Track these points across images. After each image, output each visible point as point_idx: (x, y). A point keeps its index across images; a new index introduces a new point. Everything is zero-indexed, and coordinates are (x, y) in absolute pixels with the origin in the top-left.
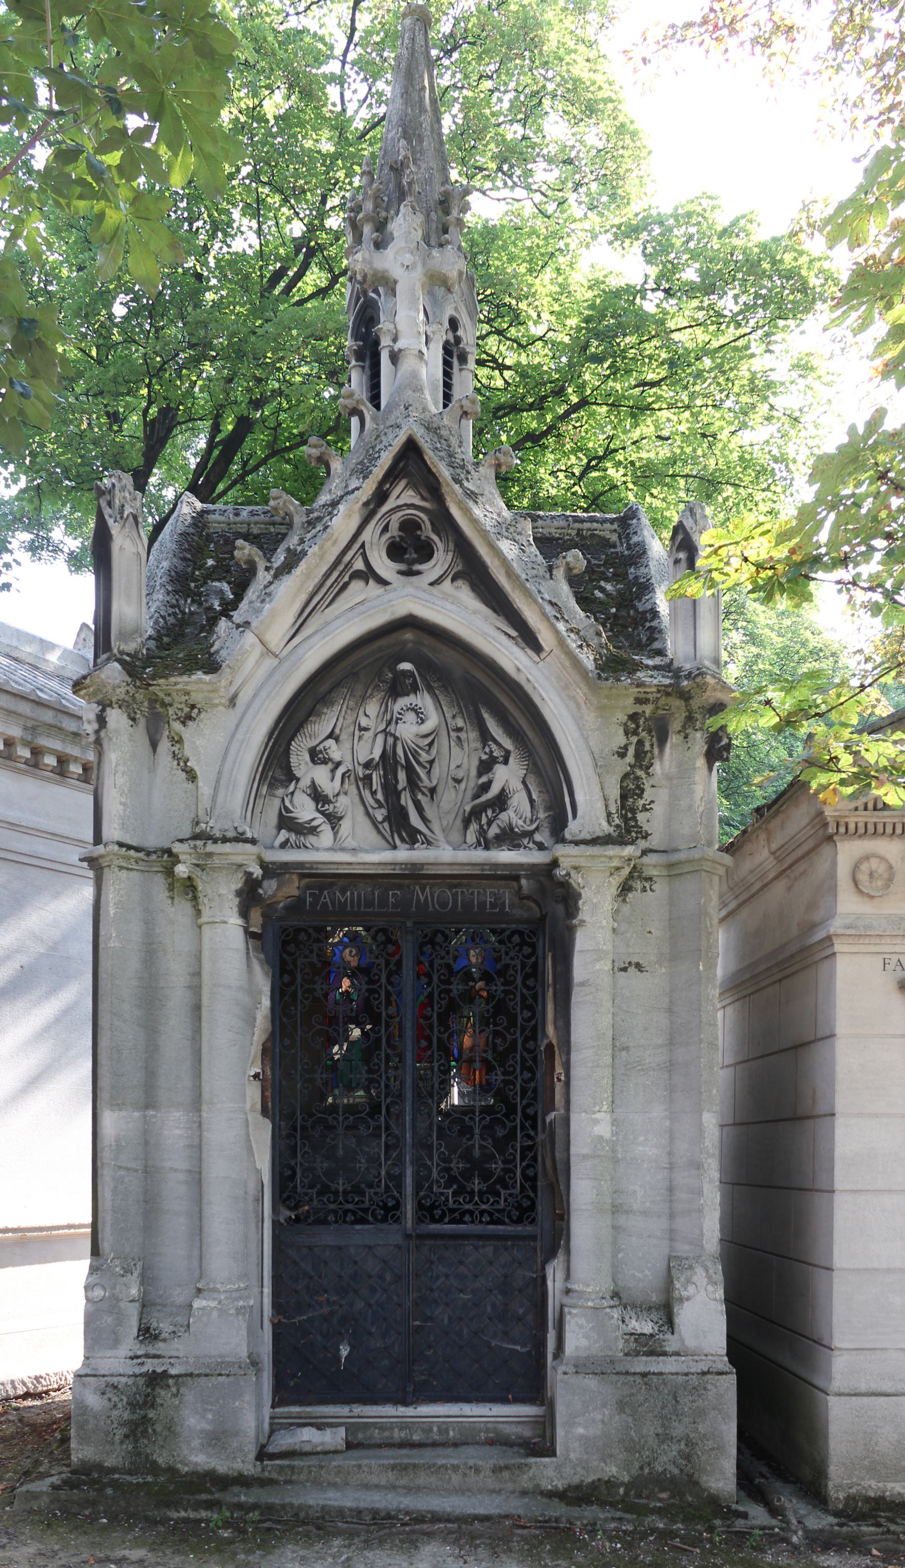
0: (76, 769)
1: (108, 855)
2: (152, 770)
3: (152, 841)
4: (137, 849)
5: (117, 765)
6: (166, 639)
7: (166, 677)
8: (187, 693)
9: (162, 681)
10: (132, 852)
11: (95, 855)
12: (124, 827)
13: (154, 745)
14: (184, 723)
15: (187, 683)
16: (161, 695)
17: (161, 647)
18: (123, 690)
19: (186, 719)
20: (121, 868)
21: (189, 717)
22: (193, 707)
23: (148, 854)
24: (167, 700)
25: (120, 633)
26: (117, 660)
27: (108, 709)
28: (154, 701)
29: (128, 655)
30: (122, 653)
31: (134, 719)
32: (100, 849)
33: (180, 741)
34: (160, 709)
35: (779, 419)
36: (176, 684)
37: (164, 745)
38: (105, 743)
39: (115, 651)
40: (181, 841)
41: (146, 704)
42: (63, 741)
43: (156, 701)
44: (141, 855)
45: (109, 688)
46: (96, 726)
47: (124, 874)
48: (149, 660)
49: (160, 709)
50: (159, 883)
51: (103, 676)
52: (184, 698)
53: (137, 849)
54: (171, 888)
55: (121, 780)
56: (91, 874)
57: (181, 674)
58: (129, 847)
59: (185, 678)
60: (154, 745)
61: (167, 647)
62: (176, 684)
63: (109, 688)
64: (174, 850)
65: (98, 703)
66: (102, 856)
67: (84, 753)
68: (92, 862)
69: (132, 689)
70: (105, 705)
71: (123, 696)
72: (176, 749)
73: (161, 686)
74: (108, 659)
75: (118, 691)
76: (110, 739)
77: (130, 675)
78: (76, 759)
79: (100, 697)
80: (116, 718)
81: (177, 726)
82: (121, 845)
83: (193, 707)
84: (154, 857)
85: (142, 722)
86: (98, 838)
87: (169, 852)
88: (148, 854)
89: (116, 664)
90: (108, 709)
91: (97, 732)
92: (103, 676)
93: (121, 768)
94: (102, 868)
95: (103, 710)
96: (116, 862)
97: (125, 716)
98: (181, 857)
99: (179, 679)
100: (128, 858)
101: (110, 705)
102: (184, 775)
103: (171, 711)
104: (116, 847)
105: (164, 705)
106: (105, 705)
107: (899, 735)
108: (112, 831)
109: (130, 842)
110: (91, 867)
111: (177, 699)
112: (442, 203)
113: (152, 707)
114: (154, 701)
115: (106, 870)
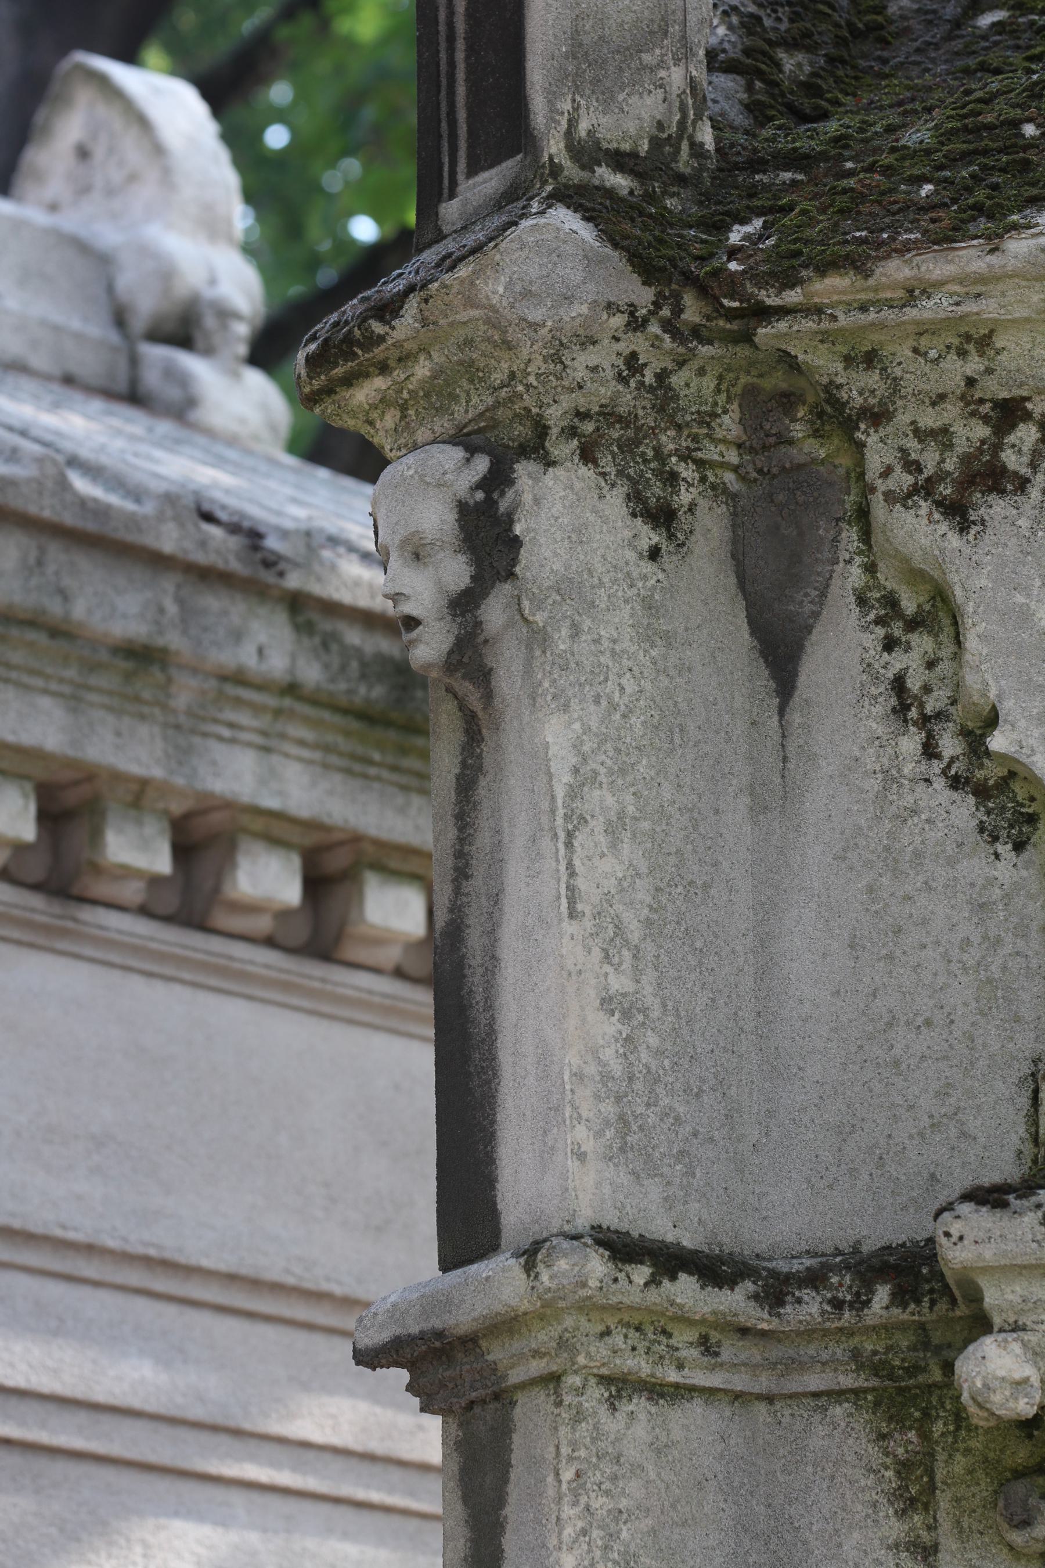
0: (137, 849)
1: (548, 1310)
2: (775, 795)
3: (791, 1216)
4: (714, 1269)
5: (582, 781)
6: (793, 64)
7: (857, 263)
8: (980, 341)
9: (832, 287)
10: (684, 1290)
11: (462, 1319)
12: (625, 1138)
13: (780, 651)
14: (957, 513)
15: (976, 286)
16: (824, 363)
17: (772, 101)
18: (605, 356)
19: (967, 491)
20: (619, 1386)
21: (989, 476)
22: (1009, 413)
23: (776, 1291)
24: (859, 387)
25: (577, 49)
26: (570, 196)
27: (524, 471)
28: (775, 401)
29: (620, 161)
30: (587, 152)
31: (662, 517)
32: (498, 1282)
33: (938, 613)
34: (807, 445)
36: (912, 294)
37: (842, 649)
39: (555, 147)
40: (991, 1197)
41: (729, 424)
42: (74, 700)
43: (787, 401)
44: (735, 1301)
45: (531, 354)
46: (456, 571)
47: (635, 1425)
48: (731, 182)
49: (807, 445)
50: (842, 1462)
51: (495, 289)
52: (955, 371)
53: (714, 1269)
54: (914, 1490)
55: (604, 868)
56: (426, 1438)
57: (946, 239)
58: (669, 1261)
59: (969, 258)
60: (780, 651)
61: (806, 106)
62: (912, 294)
63: (531, 354)
64: (955, 1256)
65: (467, 440)
66: (507, 1325)
67: (182, 755)
68: (433, 1360)
69: (653, 349)
70: (505, 448)
71: (604, 391)
72: (909, 662)
73: (819, 324)
74: (513, 200)
75: (581, 361)
76: (538, 638)
77: (647, 270)
78: (139, 795)
79: (470, 406)
81: (916, 532)
82: (622, 1248)
83: (1009, 413)
84: (811, 1307)
85: (709, 527)
86: (468, 1220)
87: (911, 1269)
88: (776, 1291)
89: (565, 219)
90: (524, 471)
91: (464, 604)
92: (495, 289)
93: (601, 800)
94: (502, 1398)
95: (498, 479)
96: (596, 1355)
97: (616, 502)
98: (996, 1297)
99: (935, 266)
100: (654, 1327)
102: (965, 811)
103: (878, 451)
104: (597, 1266)
105: (839, 418)
106: (505, 448)
107: (1040, 1481)
108: (560, 1168)
109: (661, 1227)
110: (428, 1396)
111: (916, 375)
113: (761, 441)
114: (775, 401)
115: (531, 1412)
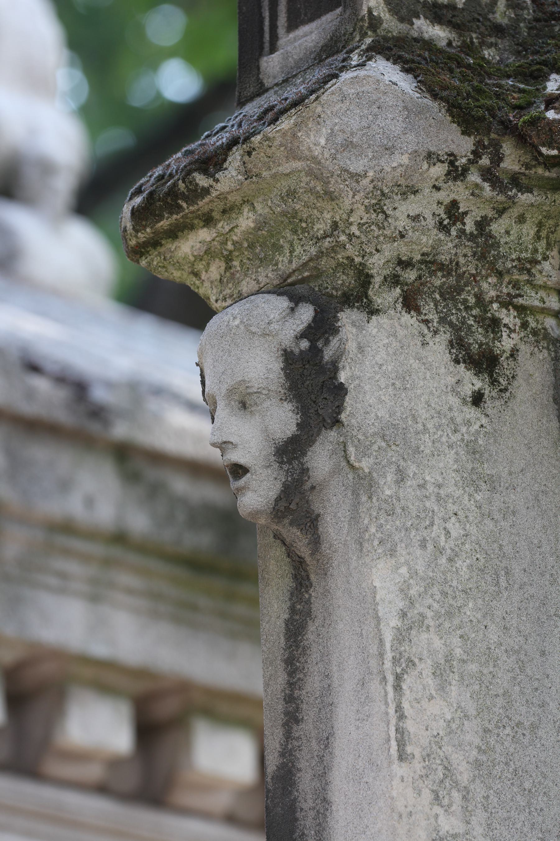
18: (427, 205)
27: (348, 319)
31: (485, 363)
35: (434, 159)
38: (335, 512)
45: (353, 204)
46: (283, 419)
51: (316, 141)
55: (430, 711)
63: (353, 204)
65: (291, 290)
69: (474, 198)
71: (425, 239)
74: (333, 54)
75: (402, 211)
79: (293, 256)
80: (392, 362)
89: (384, 70)
90: (348, 319)
91: (290, 452)
92: (316, 141)
93: (429, 643)
95: (322, 328)
97: (438, 349)
101: (358, 297)
112: (485, 731)
